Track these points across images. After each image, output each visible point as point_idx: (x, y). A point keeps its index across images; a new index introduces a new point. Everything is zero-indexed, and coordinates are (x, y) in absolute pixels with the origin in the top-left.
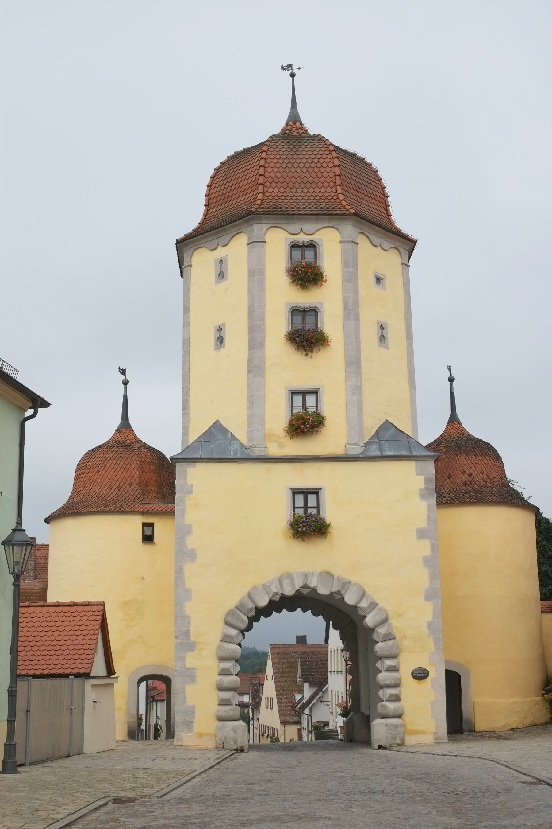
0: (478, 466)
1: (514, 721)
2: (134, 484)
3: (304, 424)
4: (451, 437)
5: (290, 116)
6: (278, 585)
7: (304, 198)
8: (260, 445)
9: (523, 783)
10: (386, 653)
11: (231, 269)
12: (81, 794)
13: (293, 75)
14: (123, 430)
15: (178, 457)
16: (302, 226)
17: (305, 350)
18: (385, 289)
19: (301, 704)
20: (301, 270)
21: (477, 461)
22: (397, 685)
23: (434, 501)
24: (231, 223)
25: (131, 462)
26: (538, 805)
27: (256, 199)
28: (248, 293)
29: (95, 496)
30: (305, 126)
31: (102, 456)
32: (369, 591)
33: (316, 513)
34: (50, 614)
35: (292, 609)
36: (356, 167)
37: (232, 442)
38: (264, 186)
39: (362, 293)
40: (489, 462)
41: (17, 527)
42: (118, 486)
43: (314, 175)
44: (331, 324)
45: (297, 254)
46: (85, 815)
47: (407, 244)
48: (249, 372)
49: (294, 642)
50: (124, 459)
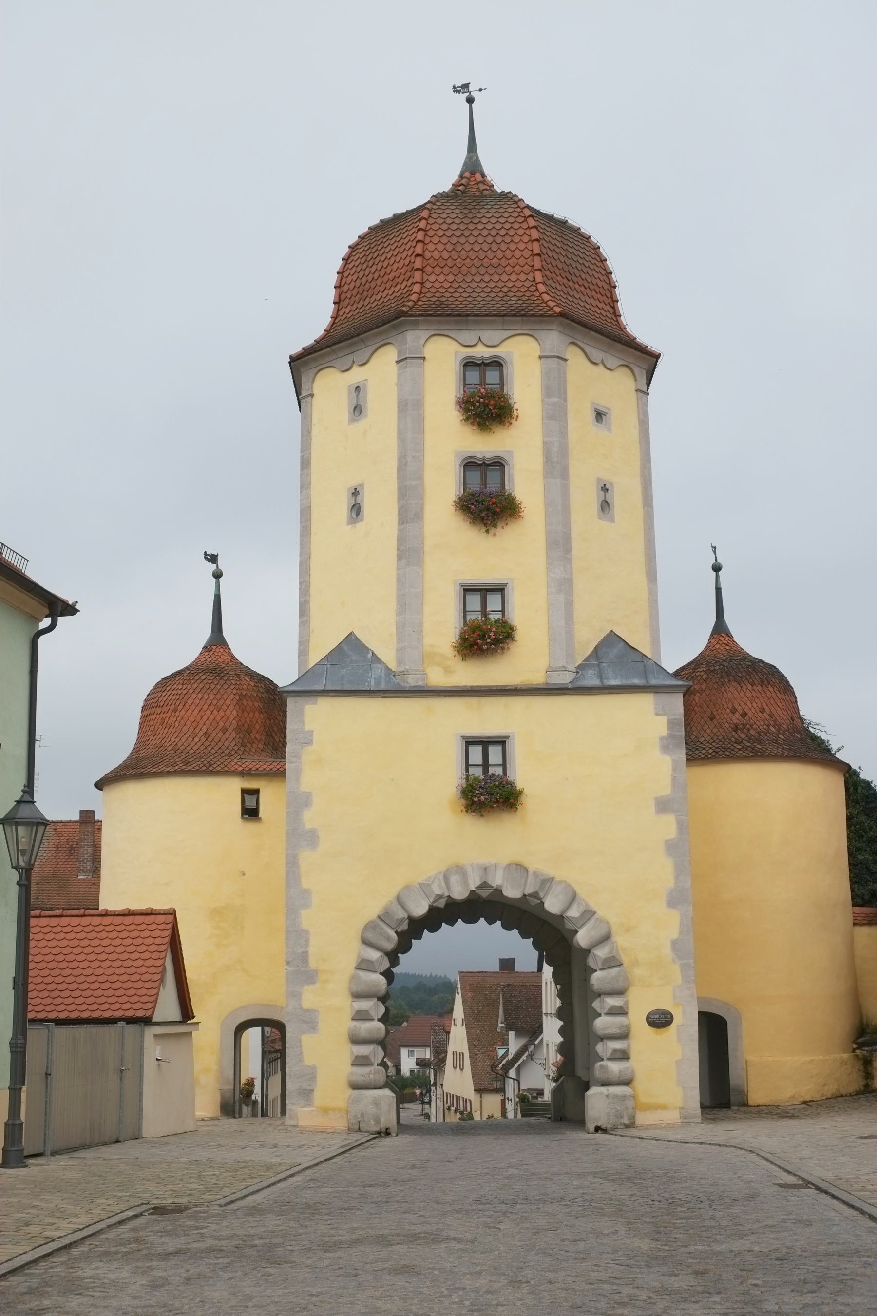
0: (757, 700)
1: (808, 1090)
2: (230, 730)
3: (483, 637)
4: (715, 657)
5: (465, 163)
6: (443, 883)
7: (485, 290)
8: (416, 670)
9: (780, 1186)
10: (607, 987)
12: (107, 1199)
13: (470, 100)
15: (291, 689)
16: (481, 334)
17: (485, 525)
18: (609, 430)
19: (504, 1062)
20: (479, 402)
21: (754, 694)
22: (624, 1036)
23: (681, 755)
24: (371, 329)
25: (225, 696)
26: (784, 1221)
27: (410, 293)
28: (398, 438)
29: (171, 748)
30: (489, 179)
32: (582, 893)
33: (501, 774)
34: (82, 928)
35: (471, 919)
36: (566, 242)
37: (374, 665)
38: (423, 272)
39: (573, 435)
40: (773, 694)
41: (22, 796)
42: (205, 733)
43: (500, 254)
44: (526, 484)
45: (474, 376)
46: (99, 1231)
47: (645, 360)
48: (399, 558)
49: (496, 968)
50: (215, 691)
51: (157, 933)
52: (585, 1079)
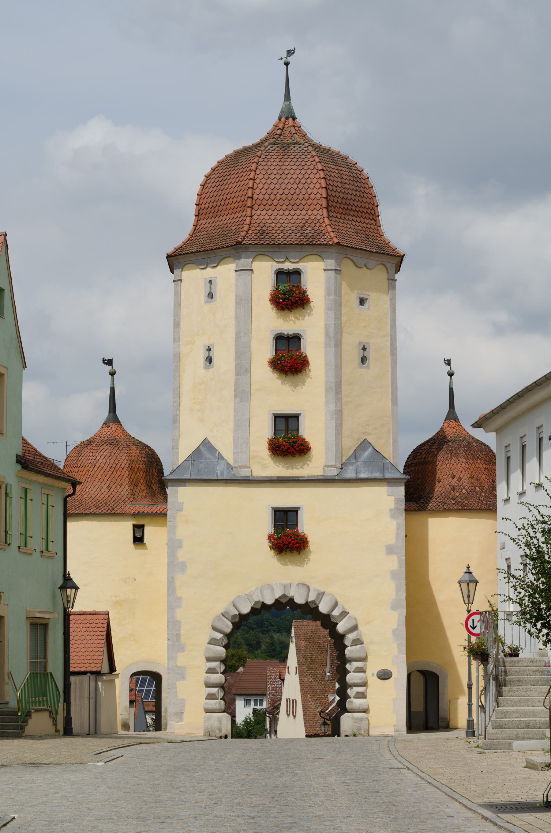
11: (219, 290)
14: (111, 424)
22: (364, 684)
31: (91, 454)
42: (109, 486)
44: (314, 348)
47: (396, 260)
48: (236, 396)
50: (114, 458)
51: (100, 625)
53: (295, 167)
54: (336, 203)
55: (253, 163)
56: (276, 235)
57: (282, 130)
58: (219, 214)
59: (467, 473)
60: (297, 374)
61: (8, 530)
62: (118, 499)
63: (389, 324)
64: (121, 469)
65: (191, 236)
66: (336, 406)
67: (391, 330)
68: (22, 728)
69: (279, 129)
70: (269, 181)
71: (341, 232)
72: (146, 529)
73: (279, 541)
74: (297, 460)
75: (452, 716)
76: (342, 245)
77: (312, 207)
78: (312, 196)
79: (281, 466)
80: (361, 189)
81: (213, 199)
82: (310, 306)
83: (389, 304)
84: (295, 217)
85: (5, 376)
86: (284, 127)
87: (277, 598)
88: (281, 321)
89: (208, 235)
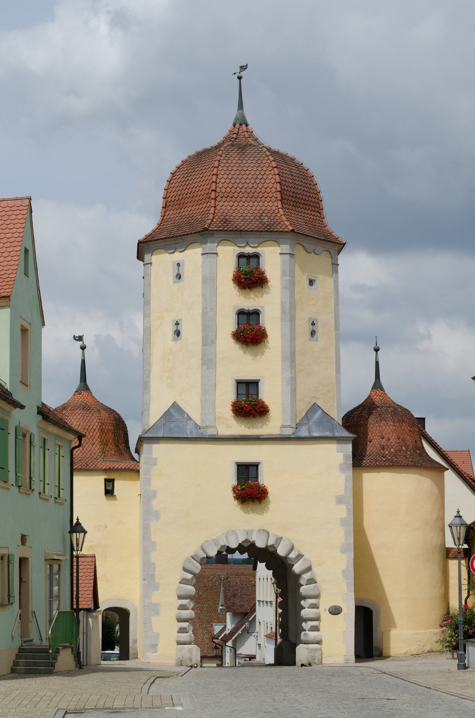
11: (186, 272)
14: (83, 392)
19: (223, 635)
44: (271, 322)
48: (203, 364)
50: (87, 421)
52: (294, 641)
53: (252, 165)
54: (288, 196)
55: (215, 161)
56: (237, 223)
57: (237, 134)
58: (185, 205)
59: (394, 434)
60: (257, 345)
61: (32, 476)
62: (91, 456)
63: (333, 303)
64: (93, 430)
65: (159, 225)
66: (291, 373)
67: (335, 308)
68: (53, 665)
69: (235, 133)
70: (230, 177)
71: (294, 221)
72: (116, 482)
73: (243, 492)
74: (257, 421)
75: (385, 646)
76: (296, 232)
77: (268, 199)
78: (268, 190)
79: (243, 426)
80: (308, 185)
81: (179, 192)
82: (268, 286)
83: (333, 285)
84: (254, 208)
85: (29, 331)
86: (238, 132)
87: (241, 542)
88: (242, 298)
89: (175, 224)
